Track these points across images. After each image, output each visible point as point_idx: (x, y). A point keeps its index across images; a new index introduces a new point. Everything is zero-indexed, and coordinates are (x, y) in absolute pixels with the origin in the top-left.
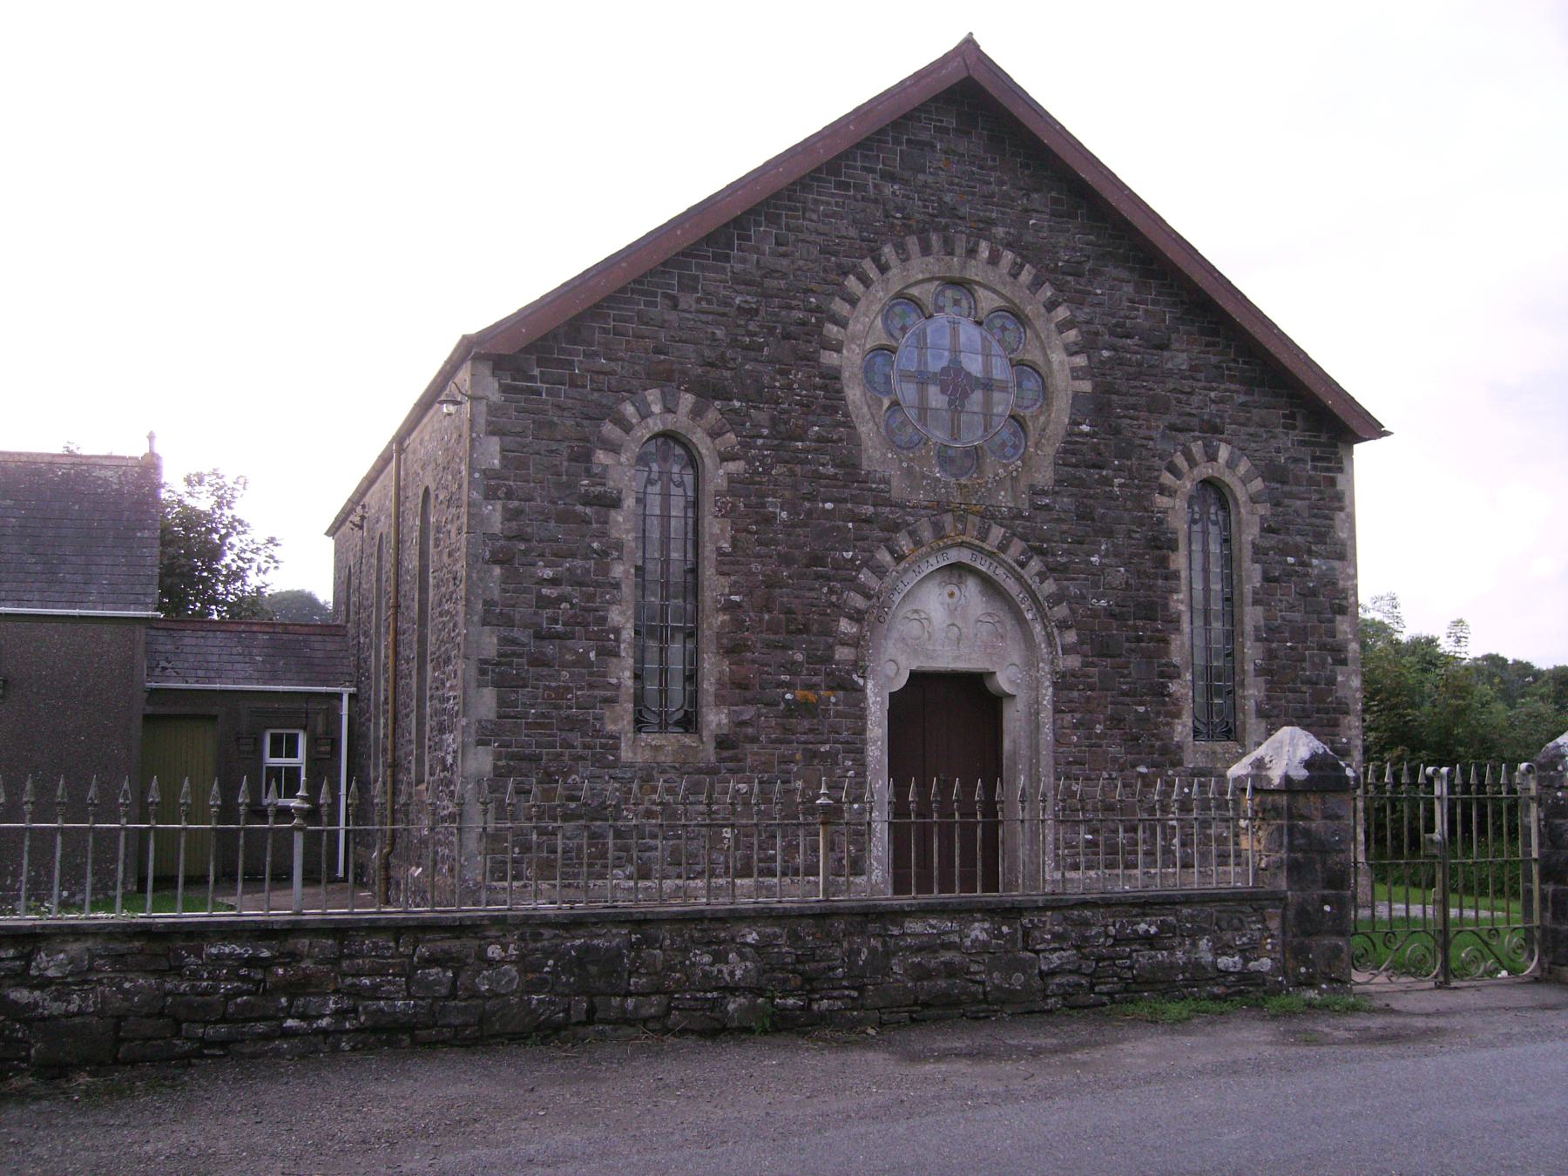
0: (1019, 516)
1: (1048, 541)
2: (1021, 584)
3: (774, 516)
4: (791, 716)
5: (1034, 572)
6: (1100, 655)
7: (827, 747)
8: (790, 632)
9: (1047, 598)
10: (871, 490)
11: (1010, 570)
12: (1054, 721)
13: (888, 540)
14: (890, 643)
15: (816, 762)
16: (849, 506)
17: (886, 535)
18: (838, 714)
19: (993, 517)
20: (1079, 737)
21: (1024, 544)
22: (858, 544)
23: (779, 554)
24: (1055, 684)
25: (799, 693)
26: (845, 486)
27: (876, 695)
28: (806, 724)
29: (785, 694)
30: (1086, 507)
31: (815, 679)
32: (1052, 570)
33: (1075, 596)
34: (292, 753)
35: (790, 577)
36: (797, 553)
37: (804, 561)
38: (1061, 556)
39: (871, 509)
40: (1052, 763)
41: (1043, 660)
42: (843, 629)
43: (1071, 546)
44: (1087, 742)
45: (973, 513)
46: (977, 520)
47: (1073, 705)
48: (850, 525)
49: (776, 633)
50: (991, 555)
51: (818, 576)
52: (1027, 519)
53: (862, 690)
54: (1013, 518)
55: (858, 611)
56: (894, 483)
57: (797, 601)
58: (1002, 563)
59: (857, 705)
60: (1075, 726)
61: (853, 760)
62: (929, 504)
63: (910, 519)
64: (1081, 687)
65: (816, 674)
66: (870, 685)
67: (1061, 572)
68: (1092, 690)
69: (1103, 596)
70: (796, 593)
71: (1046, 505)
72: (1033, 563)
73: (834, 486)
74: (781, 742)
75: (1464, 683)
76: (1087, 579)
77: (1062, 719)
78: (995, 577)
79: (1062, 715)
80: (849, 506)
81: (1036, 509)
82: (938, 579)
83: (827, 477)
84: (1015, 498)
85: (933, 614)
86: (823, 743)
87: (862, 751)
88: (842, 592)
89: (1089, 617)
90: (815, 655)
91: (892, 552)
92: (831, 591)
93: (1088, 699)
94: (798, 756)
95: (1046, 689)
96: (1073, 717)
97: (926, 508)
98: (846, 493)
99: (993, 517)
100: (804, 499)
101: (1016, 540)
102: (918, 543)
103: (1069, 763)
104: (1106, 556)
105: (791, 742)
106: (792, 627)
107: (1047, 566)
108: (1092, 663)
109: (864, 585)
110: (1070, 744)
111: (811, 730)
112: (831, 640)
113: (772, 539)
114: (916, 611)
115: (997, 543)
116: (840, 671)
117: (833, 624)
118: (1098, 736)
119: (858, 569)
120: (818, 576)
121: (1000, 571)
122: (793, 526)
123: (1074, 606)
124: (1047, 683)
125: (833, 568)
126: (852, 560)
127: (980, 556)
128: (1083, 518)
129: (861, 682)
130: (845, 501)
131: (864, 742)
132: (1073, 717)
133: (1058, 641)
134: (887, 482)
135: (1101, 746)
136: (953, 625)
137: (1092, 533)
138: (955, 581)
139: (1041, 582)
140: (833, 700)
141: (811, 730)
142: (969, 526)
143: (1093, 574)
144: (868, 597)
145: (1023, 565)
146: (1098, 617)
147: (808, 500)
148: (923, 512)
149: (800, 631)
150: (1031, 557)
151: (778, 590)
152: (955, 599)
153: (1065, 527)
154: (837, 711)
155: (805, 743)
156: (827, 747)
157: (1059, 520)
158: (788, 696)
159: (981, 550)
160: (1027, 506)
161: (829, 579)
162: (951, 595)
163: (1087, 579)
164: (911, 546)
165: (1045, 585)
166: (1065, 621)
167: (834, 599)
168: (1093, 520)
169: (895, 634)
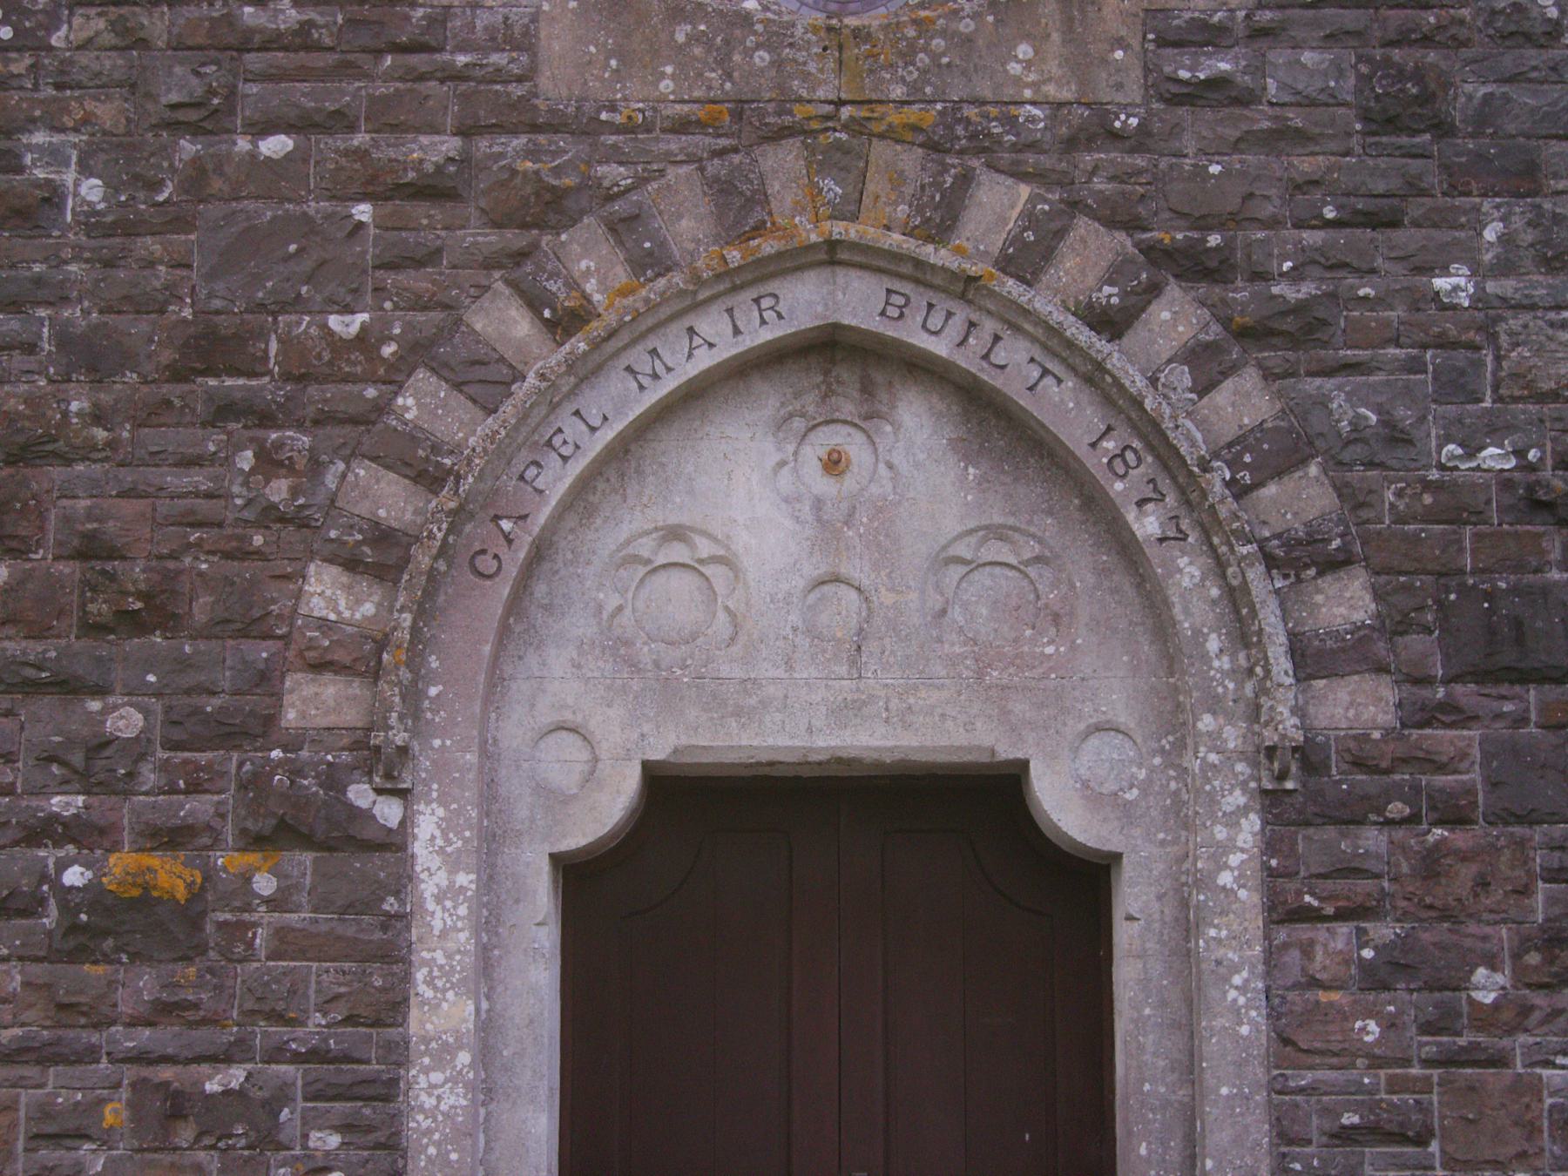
0: (1098, 131)
1: (1232, 221)
2: (1108, 401)
3: (53, 197)
4: (76, 956)
5: (1165, 347)
6: (1483, 676)
7: (236, 1076)
8: (94, 629)
9: (1232, 450)
10: (458, 76)
11: (1054, 342)
12: (1272, 957)
13: (521, 256)
14: (558, 660)
15: (185, 1134)
16: (360, 139)
17: (514, 239)
18: (286, 944)
19: (983, 145)
20: (1390, 1025)
21: (1122, 241)
22: (390, 279)
23: (64, 339)
24: (1271, 801)
25: (121, 863)
26: (346, 69)
27: (453, 864)
28: (146, 984)
29: (62, 866)
30: (1401, 75)
31: (197, 807)
32: (1252, 334)
33: (1358, 431)
34: (378, 1063)
35: (98, 417)
36: (137, 327)
37: (167, 356)
38: (1296, 276)
39: (450, 145)
40: (1261, 1134)
41: (1214, 704)
42: (317, 606)
43: (1341, 237)
44: (1430, 1046)
45: (888, 135)
46: (910, 160)
47: (1365, 885)
48: (363, 212)
49: (39, 632)
50: (966, 287)
51: (224, 411)
52: (1140, 141)
53: (395, 843)
54: (1071, 144)
55: (382, 536)
56: (555, 43)
57: (130, 507)
58: (1016, 319)
59: (369, 905)
60: (1375, 979)
61: (345, 1128)
62: (700, 112)
63: (614, 174)
64: (1397, 809)
65: (194, 788)
66: (427, 825)
67: (1295, 341)
68: (1456, 818)
69: (1495, 430)
70: (128, 477)
71: (1217, 83)
72: (1161, 312)
73: (303, 74)
74: (46, 1055)
75: (1261, 269)
76: (1416, 366)
77: (1307, 950)
78: (987, 376)
79: (1303, 931)
80: (360, 139)
81: (1174, 101)
82: (769, 398)
83: (273, 42)
84: (1081, 64)
85: (743, 541)
86: (223, 1058)
87: (387, 1091)
88: (316, 467)
89: (1429, 517)
90: (197, 711)
91: (534, 302)
92: (269, 462)
93: (1431, 864)
94: (114, 1114)
95: (1232, 819)
96: (1362, 939)
97: (682, 126)
98: (349, 93)
99: (983, 145)
100: (175, 127)
101: (1083, 226)
102: (652, 263)
103: (1345, 1136)
104: (1504, 268)
105: (90, 1055)
106: (100, 608)
107: (1226, 322)
108: (1449, 706)
109: (413, 436)
110: (1345, 1055)
111: (163, 1011)
112: (263, 652)
113: (38, 281)
114: (675, 534)
115: (996, 242)
116: (296, 772)
117: (273, 590)
118: (1485, 1018)
119: (395, 377)
120: (224, 411)
121: (1015, 353)
122: (128, 228)
123: (1357, 474)
124: (1238, 798)
125: (287, 377)
126: (365, 341)
127: (920, 298)
128: (1391, 123)
129: (389, 812)
130: (341, 121)
131: (399, 1054)
132: (1362, 939)
133: (1270, 618)
134: (522, 40)
135: (1499, 1061)
136: (836, 579)
137: (1434, 180)
138: (848, 409)
139: (1204, 388)
140: (265, 884)
141: (163, 1011)
142: (876, 185)
143: (1443, 343)
144: (429, 478)
145: (1111, 323)
146: (1479, 516)
147: (196, 130)
148: (674, 144)
149: (135, 623)
150: (1154, 290)
151: (57, 472)
152: (850, 483)
153: (1306, 165)
154: (281, 933)
155: (141, 1058)
156: (236, 1076)
157: (1281, 138)
158: (74, 876)
159: (920, 274)
160: (1134, 92)
161: (266, 419)
162: (834, 464)
163: (1416, 366)
164: (621, 275)
165: (1222, 396)
166: (1314, 538)
167: (278, 490)
168: (1442, 129)
169: (579, 625)
